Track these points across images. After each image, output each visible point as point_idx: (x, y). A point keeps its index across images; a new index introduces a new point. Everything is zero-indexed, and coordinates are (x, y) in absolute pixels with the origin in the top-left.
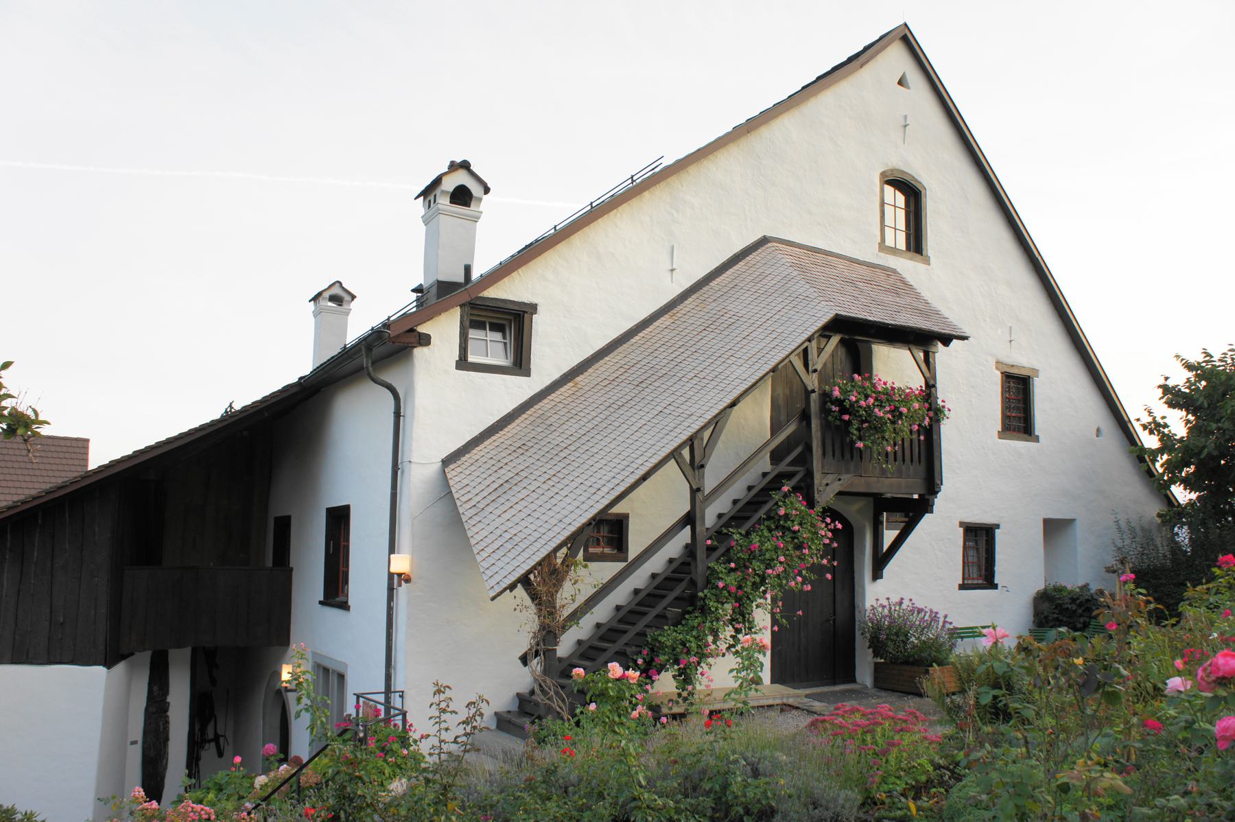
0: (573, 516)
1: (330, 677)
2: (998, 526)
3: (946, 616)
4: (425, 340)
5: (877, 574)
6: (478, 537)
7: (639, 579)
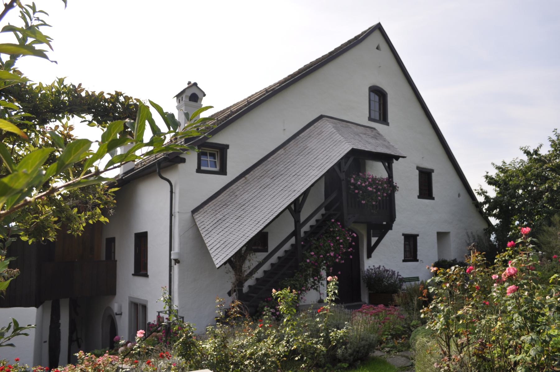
0: (249, 233)
1: (139, 309)
2: (418, 235)
3: (398, 273)
4: (183, 161)
5: (369, 256)
6: (210, 243)
7: (274, 260)
